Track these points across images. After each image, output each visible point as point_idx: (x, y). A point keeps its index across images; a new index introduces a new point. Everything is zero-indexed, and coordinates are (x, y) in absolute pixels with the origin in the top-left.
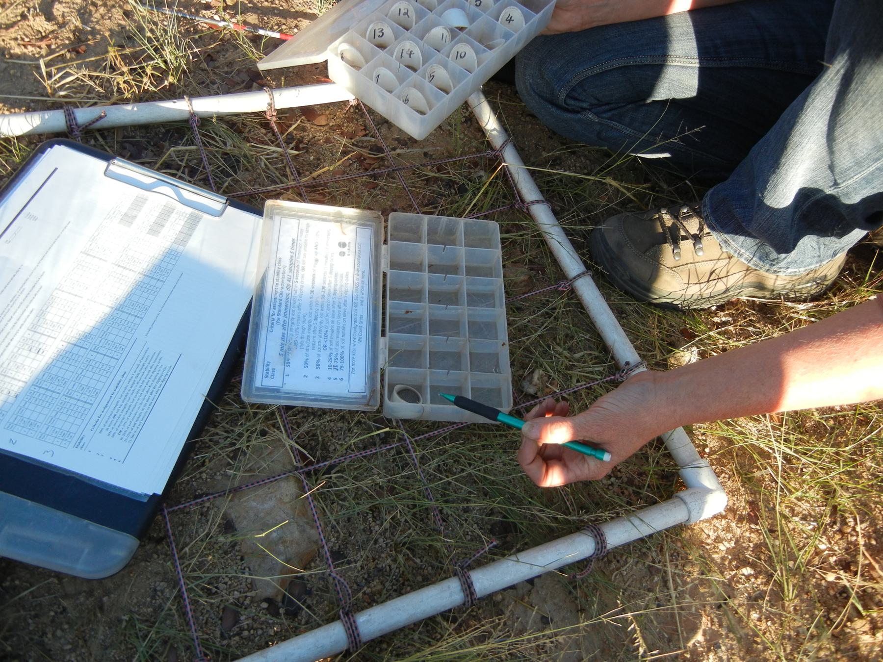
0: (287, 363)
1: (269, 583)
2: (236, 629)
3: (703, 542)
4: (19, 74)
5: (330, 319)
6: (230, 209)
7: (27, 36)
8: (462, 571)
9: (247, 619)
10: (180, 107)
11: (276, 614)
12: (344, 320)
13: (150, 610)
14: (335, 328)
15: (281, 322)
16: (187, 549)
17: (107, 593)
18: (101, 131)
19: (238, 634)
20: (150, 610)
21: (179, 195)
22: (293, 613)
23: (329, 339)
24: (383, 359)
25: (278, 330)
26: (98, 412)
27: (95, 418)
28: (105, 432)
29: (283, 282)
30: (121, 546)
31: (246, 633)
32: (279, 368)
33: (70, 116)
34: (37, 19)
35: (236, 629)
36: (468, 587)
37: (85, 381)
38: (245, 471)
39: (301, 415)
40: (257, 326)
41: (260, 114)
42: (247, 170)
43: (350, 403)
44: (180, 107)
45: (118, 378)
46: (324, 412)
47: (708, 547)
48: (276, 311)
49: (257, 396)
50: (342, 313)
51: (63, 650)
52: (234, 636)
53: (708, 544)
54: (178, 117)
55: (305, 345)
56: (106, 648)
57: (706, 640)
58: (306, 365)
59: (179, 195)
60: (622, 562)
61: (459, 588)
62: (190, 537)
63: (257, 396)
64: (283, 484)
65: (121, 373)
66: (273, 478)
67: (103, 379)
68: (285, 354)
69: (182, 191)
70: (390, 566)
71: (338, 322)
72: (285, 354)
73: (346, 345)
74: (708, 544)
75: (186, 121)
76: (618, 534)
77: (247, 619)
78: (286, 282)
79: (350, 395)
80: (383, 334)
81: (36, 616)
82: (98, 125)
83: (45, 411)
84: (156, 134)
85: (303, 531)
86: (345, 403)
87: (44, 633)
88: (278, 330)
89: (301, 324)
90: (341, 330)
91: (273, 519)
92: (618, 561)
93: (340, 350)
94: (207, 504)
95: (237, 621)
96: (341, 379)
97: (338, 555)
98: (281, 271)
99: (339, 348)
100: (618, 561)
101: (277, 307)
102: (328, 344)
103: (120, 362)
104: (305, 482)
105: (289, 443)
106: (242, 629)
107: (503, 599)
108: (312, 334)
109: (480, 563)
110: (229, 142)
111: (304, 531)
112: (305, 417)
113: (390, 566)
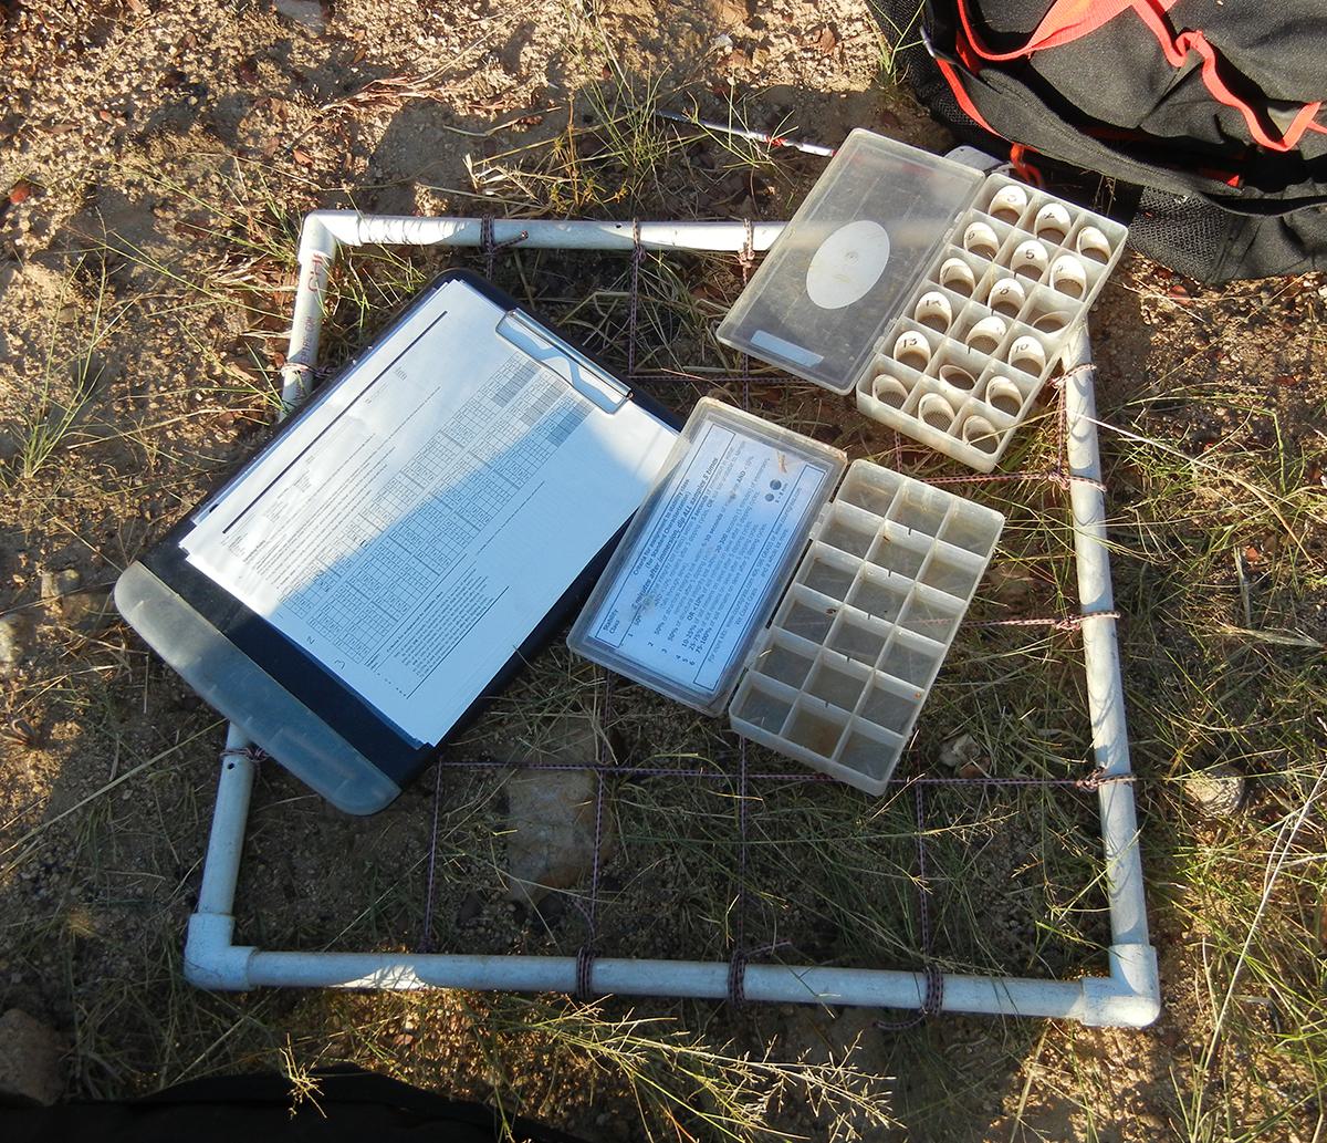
0: (636, 619)
1: (523, 886)
3: (1108, 1058)
4: (453, 150)
5: (715, 580)
6: (631, 408)
7: (478, 94)
8: (739, 955)
9: (489, 915)
10: (621, 234)
11: (520, 923)
12: (731, 589)
13: (396, 865)
14: (715, 596)
15: (653, 565)
16: (448, 815)
18: (521, 250)
19: (474, 928)
20: (396, 865)
21: (575, 374)
22: (538, 931)
23: (700, 607)
24: (757, 654)
25: (644, 574)
27: (395, 638)
28: (400, 657)
29: (677, 513)
30: (383, 789)
31: (482, 930)
32: (625, 622)
33: (487, 228)
34: (494, 72)
36: (736, 981)
38: (542, 747)
39: (634, 697)
40: (622, 561)
41: (732, 255)
42: (688, 336)
43: (693, 699)
44: (621, 234)
46: (662, 701)
47: (1112, 1068)
48: (653, 549)
50: (733, 578)
51: (306, 873)
52: (469, 928)
53: (1114, 1064)
54: (618, 245)
55: (668, 606)
56: (344, 888)
58: (657, 631)
59: (575, 374)
60: (972, 1035)
61: (725, 978)
62: (459, 801)
63: (589, 650)
64: (574, 777)
65: (437, 592)
66: (568, 765)
67: (417, 594)
68: (639, 609)
69: (581, 369)
70: (668, 920)
71: (722, 589)
72: (639, 609)
73: (718, 623)
74: (1114, 1064)
75: (630, 252)
76: (966, 995)
77: (489, 915)
78: (681, 515)
79: (694, 687)
80: (768, 626)
81: (293, 828)
82: (519, 244)
84: (590, 262)
85: (579, 840)
86: (684, 695)
87: (295, 849)
88: (644, 574)
89: (676, 576)
90: (721, 600)
91: (552, 809)
92: (968, 1032)
93: (708, 626)
94: (488, 771)
95: (478, 913)
96: (692, 663)
97: (611, 883)
98: (682, 498)
99: (708, 622)
100: (968, 1032)
101: (656, 544)
102: (696, 613)
103: (441, 578)
104: (602, 783)
105: (598, 731)
107: (794, 1015)
108: (682, 594)
109: (766, 960)
110: (675, 291)
111: (582, 841)
112: (636, 701)
113: (668, 920)
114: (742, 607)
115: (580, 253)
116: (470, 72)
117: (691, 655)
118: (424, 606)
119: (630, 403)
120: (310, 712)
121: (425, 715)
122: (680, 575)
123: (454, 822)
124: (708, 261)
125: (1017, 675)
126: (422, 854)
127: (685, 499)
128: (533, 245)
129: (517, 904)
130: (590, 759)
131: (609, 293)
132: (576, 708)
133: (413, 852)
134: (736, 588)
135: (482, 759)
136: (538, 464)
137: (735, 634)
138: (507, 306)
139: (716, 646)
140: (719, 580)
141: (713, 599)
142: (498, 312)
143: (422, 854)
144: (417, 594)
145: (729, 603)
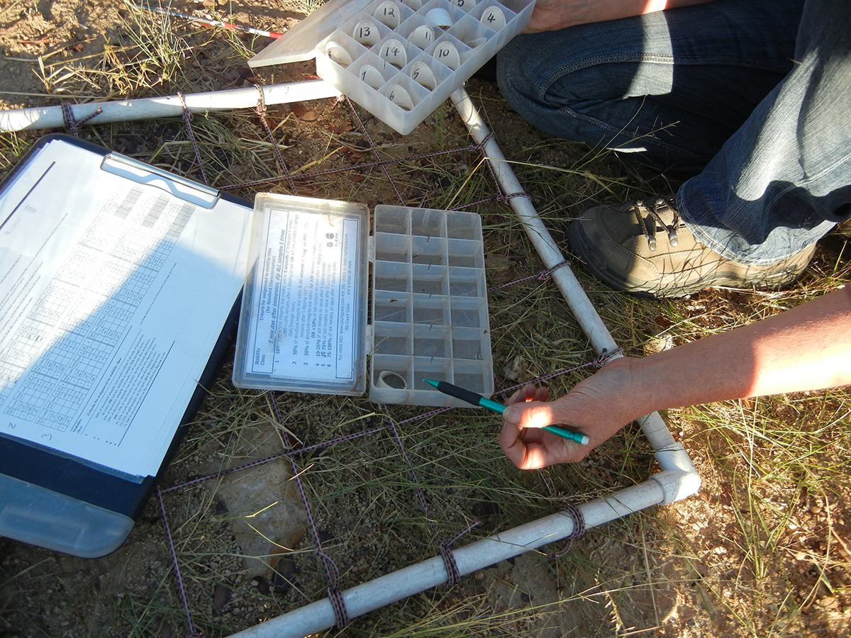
0: (276, 349)
1: (259, 562)
2: (227, 606)
4: (18, 71)
7: (26, 35)
8: (446, 550)
15: (271, 310)
16: (180, 529)
17: (103, 572)
18: (97, 126)
19: (230, 611)
21: (172, 187)
24: (369, 346)
25: (268, 318)
26: (95, 397)
30: (117, 526)
31: (237, 610)
32: (269, 355)
33: (67, 112)
34: (36, 18)
35: (227, 606)
36: (451, 566)
37: (82, 367)
39: (290, 400)
40: (248, 314)
41: (250, 110)
42: (238, 164)
44: (173, 103)
45: (114, 364)
47: (682, 527)
49: (248, 382)
52: (226, 613)
53: (682, 525)
54: (171, 113)
57: (680, 617)
58: (295, 352)
59: (172, 187)
60: (599, 542)
61: (443, 566)
63: (248, 382)
64: (272, 466)
66: (263, 461)
67: (99, 365)
68: (275, 341)
70: (376, 546)
71: (326, 311)
72: (275, 341)
73: (334, 333)
74: (682, 525)
75: (180, 117)
76: (595, 515)
79: (337, 381)
80: (369, 323)
81: (35, 594)
82: (95, 120)
83: (44, 396)
87: (43, 610)
88: (268, 318)
91: (263, 500)
92: (596, 541)
94: (200, 486)
95: (228, 599)
97: (325, 535)
99: (327, 335)
100: (596, 541)
101: (267, 296)
106: (233, 607)
109: (463, 543)
110: (221, 137)
112: (293, 402)
114: (345, 317)
115: (141, 123)
116: (14, 23)
117: (326, 361)
118: (109, 373)
119: (221, 200)
120: (29, 485)
121: (138, 452)
122: (293, 310)
123: (185, 535)
124: (234, 119)
125: (527, 315)
126: (165, 570)
127: (274, 261)
128: (107, 119)
129: (258, 578)
130: (279, 450)
131: (174, 142)
132: (254, 417)
133: (156, 570)
134: (335, 306)
135: (189, 479)
136: (146, 286)
137: (348, 338)
138: (103, 152)
139: (340, 348)
140: (321, 305)
141: (323, 319)
142: (99, 158)
143: (165, 570)
144: (99, 365)
145: (335, 319)
